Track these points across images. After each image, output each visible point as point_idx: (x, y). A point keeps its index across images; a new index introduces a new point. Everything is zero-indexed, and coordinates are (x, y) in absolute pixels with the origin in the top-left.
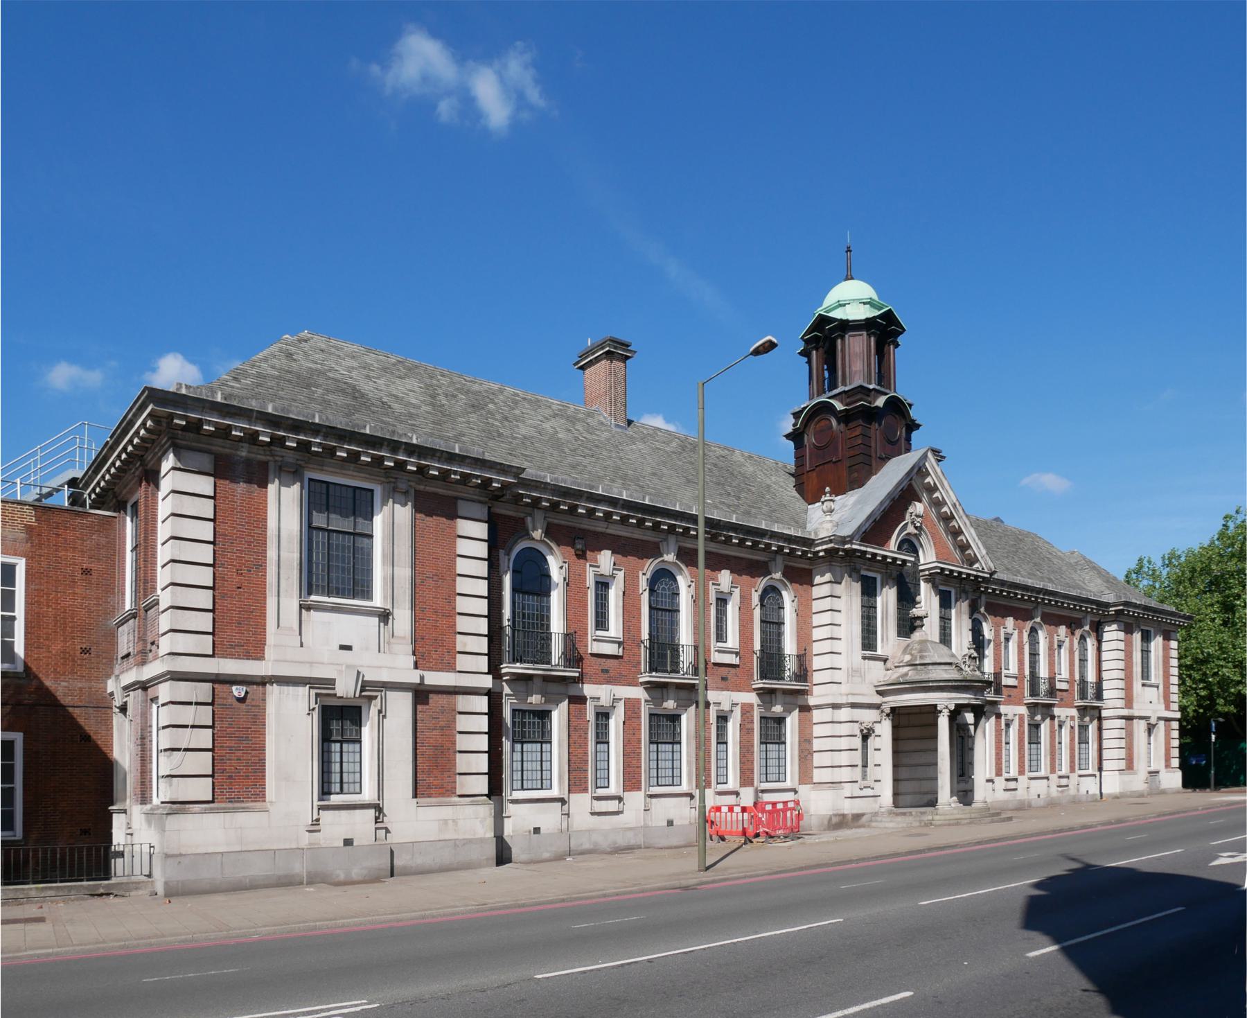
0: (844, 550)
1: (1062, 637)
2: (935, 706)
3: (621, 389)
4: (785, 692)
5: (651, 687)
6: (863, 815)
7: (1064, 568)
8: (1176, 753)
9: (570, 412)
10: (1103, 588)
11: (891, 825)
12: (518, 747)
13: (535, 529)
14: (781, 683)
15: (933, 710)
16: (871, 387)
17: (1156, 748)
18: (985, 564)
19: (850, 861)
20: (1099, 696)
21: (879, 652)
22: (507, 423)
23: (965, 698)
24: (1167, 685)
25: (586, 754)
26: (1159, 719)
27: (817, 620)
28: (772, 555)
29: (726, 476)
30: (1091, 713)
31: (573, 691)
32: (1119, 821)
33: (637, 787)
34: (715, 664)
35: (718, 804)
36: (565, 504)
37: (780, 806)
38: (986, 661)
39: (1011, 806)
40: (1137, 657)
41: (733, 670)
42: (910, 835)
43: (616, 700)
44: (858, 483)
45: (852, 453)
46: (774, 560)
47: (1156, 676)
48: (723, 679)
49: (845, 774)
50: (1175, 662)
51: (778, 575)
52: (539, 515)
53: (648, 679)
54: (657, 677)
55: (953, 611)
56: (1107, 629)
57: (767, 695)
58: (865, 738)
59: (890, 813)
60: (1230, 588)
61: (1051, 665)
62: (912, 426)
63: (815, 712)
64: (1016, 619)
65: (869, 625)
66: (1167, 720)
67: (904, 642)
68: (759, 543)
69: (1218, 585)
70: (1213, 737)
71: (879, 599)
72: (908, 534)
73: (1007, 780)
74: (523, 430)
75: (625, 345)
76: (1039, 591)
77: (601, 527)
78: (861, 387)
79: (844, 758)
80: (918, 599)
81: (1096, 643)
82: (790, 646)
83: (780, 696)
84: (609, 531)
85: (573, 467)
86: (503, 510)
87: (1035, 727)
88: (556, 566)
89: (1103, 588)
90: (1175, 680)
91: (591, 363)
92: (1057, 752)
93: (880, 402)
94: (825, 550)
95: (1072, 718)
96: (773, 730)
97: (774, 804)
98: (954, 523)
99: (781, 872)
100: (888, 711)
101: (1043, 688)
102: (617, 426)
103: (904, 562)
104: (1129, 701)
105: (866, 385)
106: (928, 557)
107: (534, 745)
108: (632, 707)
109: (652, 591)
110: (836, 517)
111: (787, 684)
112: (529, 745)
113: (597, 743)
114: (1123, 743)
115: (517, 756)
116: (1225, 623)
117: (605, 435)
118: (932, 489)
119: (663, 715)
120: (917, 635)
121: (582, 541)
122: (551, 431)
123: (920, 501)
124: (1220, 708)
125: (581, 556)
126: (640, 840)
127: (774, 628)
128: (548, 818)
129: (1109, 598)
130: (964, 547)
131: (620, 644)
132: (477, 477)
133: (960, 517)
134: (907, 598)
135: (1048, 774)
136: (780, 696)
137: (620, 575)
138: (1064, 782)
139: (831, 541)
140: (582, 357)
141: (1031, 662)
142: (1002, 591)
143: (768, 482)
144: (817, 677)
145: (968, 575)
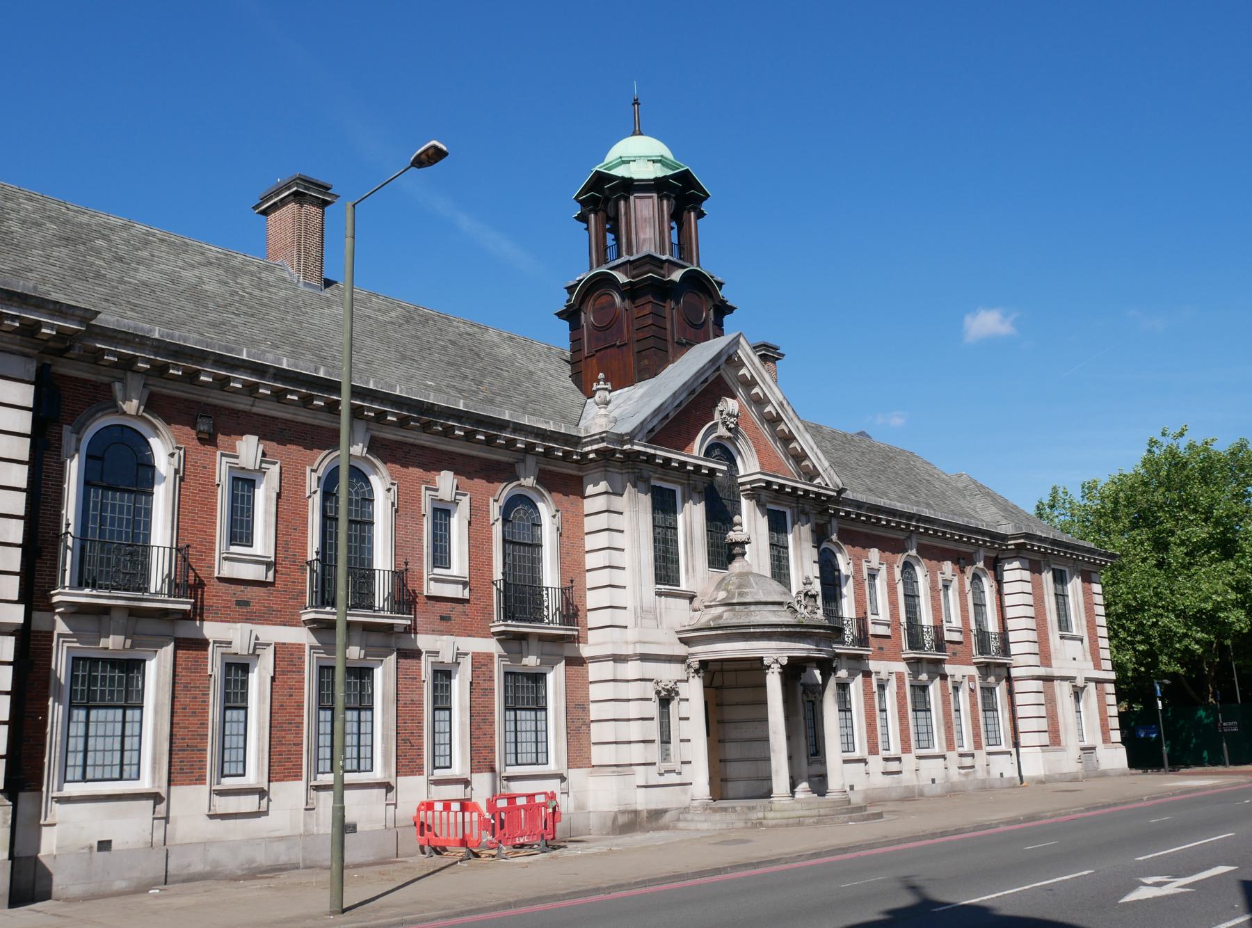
0: (623, 452)
1: (948, 575)
2: (761, 659)
3: (315, 239)
4: (542, 638)
5: (506, 639)
6: (665, 811)
7: (949, 493)
8: (1115, 723)
9: (234, 263)
10: (999, 518)
11: (705, 826)
12: (80, 714)
13: (127, 398)
14: (535, 626)
15: (757, 666)
16: (664, 258)
17: (1088, 718)
18: (829, 479)
19: (597, 890)
20: (1005, 649)
21: (684, 586)
22: (118, 265)
23: (801, 649)
24: (1094, 639)
25: (204, 724)
26: (1088, 680)
27: (590, 542)
28: (520, 456)
29: (467, 355)
30: (996, 669)
31: (184, 630)
32: (1030, 818)
33: (417, 770)
34: (430, 598)
35: (434, 797)
36: (177, 367)
37: (521, 801)
39: (894, 795)
40: (1050, 602)
41: (459, 607)
43: (460, 654)
44: (649, 371)
45: (640, 335)
46: (523, 461)
47: (1078, 625)
48: (442, 618)
49: (636, 753)
50: (1101, 610)
51: (529, 481)
52: (135, 382)
54: (513, 626)
55: (790, 537)
56: (1007, 567)
58: (665, 702)
59: (706, 808)
60: (1161, 523)
61: (936, 609)
62: (723, 309)
63: (592, 667)
64: (882, 550)
65: (666, 551)
66: (1098, 682)
67: (718, 574)
68: (497, 437)
69: (1146, 519)
70: (1160, 703)
71: (680, 518)
72: (720, 437)
73: (886, 759)
74: (143, 274)
75: (325, 188)
76: (911, 516)
77: (243, 404)
78: (649, 256)
79: (634, 731)
80: (736, 519)
81: (994, 584)
82: (550, 576)
83: (534, 644)
84: (255, 410)
85: (213, 325)
86: (65, 368)
87: (921, 690)
88: (163, 452)
89: (999, 518)
90: (1103, 632)
91: (275, 207)
92: (955, 722)
93: (676, 276)
94: (596, 451)
95: (971, 678)
96: (525, 692)
97: (531, 797)
99: (470, 912)
100: (696, 665)
101: (928, 638)
102: (306, 284)
104: (1045, 657)
105: (658, 255)
106: (749, 467)
107: (111, 712)
108: (481, 663)
109: (506, 521)
110: (619, 410)
111: (551, 625)
112: (102, 712)
113: (435, 709)
114: (1042, 711)
115: (77, 729)
116: (1160, 565)
117: (283, 293)
118: (749, 383)
120: (736, 566)
121: (210, 420)
122: (194, 280)
123: (734, 397)
124: (1163, 668)
125: (208, 440)
126: (296, 855)
127: (520, 551)
128: (129, 827)
129: (1007, 529)
131: (268, 565)
132: (13, 318)
133: (791, 420)
134: (720, 516)
135: (944, 752)
136: (534, 644)
137: (274, 471)
138: (967, 761)
139: (603, 440)
140: (265, 199)
141: (907, 606)
142: (858, 515)
143: (532, 368)
144: (593, 619)
145: (806, 492)
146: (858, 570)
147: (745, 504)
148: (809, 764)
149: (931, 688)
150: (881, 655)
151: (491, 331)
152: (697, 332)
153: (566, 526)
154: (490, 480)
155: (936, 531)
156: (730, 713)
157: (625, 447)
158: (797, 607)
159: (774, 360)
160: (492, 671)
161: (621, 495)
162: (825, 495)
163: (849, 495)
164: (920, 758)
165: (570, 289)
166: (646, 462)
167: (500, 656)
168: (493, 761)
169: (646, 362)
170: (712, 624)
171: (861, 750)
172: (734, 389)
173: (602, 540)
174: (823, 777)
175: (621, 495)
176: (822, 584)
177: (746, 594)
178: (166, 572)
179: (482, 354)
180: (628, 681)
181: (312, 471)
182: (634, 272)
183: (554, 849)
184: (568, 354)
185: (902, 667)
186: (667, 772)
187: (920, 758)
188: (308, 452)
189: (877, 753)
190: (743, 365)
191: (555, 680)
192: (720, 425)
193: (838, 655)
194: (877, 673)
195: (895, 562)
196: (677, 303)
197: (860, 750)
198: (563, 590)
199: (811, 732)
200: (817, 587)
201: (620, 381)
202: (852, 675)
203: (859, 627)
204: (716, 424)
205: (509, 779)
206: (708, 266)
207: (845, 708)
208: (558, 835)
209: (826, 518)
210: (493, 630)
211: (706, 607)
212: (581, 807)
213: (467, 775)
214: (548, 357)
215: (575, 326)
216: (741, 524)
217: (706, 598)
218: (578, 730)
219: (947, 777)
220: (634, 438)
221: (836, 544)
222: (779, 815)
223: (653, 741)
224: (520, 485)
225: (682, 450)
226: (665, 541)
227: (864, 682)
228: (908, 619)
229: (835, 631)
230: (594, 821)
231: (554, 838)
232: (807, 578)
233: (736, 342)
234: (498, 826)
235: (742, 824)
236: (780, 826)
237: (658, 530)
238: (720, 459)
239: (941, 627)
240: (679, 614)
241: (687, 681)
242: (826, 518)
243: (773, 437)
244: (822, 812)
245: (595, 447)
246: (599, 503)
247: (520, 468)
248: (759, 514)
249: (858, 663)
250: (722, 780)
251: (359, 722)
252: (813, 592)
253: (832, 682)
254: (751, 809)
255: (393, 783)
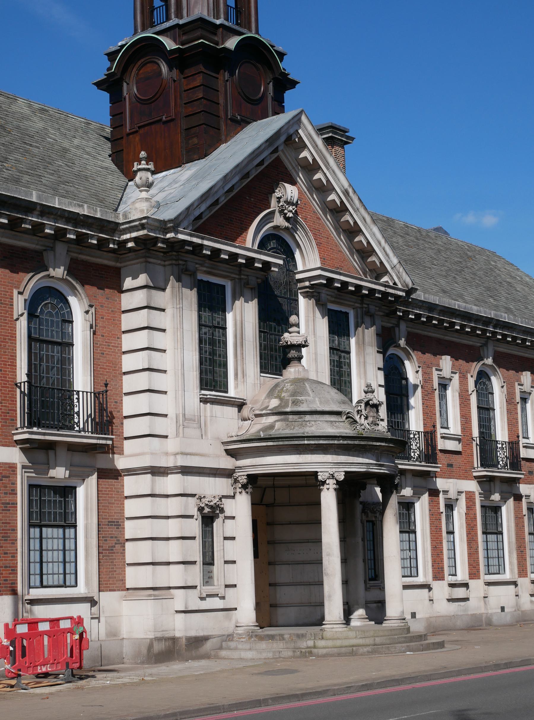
0: (165, 241)
2: (316, 474)
4: (72, 447)
5: (29, 447)
6: (206, 639)
11: (249, 655)
15: (311, 482)
16: (218, 22)
18: (398, 276)
21: (232, 393)
23: (360, 464)
27: (128, 342)
37: (44, 627)
38: (412, 414)
39: (459, 623)
42: (267, 673)
44: (200, 152)
46: (53, 249)
49: (175, 576)
51: (59, 272)
53: (26, 436)
54: (39, 434)
55: (353, 341)
57: (39, 452)
59: (251, 635)
61: (512, 424)
62: (285, 83)
64: (455, 357)
65: (213, 353)
67: (270, 380)
68: (22, 221)
71: (230, 316)
72: (276, 227)
73: (452, 585)
76: (487, 321)
78: (201, 20)
79: (173, 551)
82: (82, 379)
83: (62, 453)
87: (492, 511)
93: (232, 43)
94: (135, 239)
97: (54, 622)
98: (347, 217)
100: (243, 480)
101: (502, 455)
103: (267, 265)
105: (211, 19)
106: (308, 261)
109: (32, 316)
118: (311, 168)
119: (49, 487)
123: (293, 183)
130: (365, 252)
133: (357, 210)
134: (275, 316)
135: (516, 578)
136: (62, 453)
139: (143, 227)
141: (480, 419)
142: (430, 319)
143: (66, 144)
144: (130, 427)
145: (372, 291)
146: (427, 379)
147: (303, 302)
148: (367, 589)
149: (504, 509)
150: (451, 472)
151: (20, 101)
152: (255, 108)
153: (100, 324)
154: (14, 270)
155: (514, 338)
156: (281, 533)
157: (169, 236)
158: (357, 418)
159: (343, 144)
160: (14, 484)
161: (164, 290)
162: (392, 295)
163: (419, 295)
164: (489, 584)
165: (111, 56)
166: (192, 252)
167: (24, 467)
168: (15, 582)
169: (195, 140)
170: (262, 435)
171: (425, 575)
172: (294, 173)
173: (140, 339)
174: (381, 604)
175: (164, 290)
176: (387, 393)
177: (301, 402)
178: (89, 412)
179: (9, 127)
180: (167, 496)
181: (19, 293)
182: (184, 38)
183: (81, 678)
184: (108, 130)
185: (472, 486)
186: (209, 596)
187: (489, 584)
188: (15, 275)
189: (442, 579)
190: (305, 146)
191: (86, 494)
192: (277, 214)
193: (403, 472)
194: (446, 492)
195: (468, 371)
196: (232, 74)
197: (424, 574)
198: (96, 395)
199: (370, 555)
200: (380, 395)
201: (164, 162)
202: (417, 494)
203: (426, 440)
204: (273, 212)
205: (33, 602)
206: (269, 32)
207: (407, 528)
208: (86, 663)
209: (394, 321)
210: (16, 438)
211: (257, 416)
212: (113, 634)
213: (94, 592)
214: (86, 133)
215: (116, 99)
216: (298, 325)
217: (257, 406)
218: (111, 549)
219: (518, 606)
220: (178, 225)
221: (404, 349)
222: (330, 643)
223: (194, 563)
224: (48, 276)
225: (234, 240)
226: (212, 342)
227: (431, 502)
228: (481, 433)
229: (399, 444)
230: (127, 650)
231: (80, 667)
232: (369, 386)
233: (296, 121)
234: (19, 653)
235: (290, 653)
236: (332, 655)
237: (204, 330)
238: (276, 252)
239: (518, 443)
240: (226, 423)
241: (233, 497)
242: (394, 321)
243: (336, 229)
244: (378, 640)
245: (134, 235)
246: (138, 298)
247: (49, 257)
248: (318, 314)
249: (424, 482)
250: (271, 606)
251: (64, 538)
252: (375, 401)
253: (394, 501)
254: (301, 637)
255: (96, 598)
